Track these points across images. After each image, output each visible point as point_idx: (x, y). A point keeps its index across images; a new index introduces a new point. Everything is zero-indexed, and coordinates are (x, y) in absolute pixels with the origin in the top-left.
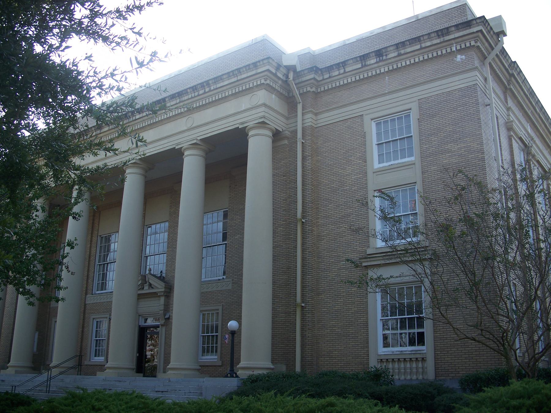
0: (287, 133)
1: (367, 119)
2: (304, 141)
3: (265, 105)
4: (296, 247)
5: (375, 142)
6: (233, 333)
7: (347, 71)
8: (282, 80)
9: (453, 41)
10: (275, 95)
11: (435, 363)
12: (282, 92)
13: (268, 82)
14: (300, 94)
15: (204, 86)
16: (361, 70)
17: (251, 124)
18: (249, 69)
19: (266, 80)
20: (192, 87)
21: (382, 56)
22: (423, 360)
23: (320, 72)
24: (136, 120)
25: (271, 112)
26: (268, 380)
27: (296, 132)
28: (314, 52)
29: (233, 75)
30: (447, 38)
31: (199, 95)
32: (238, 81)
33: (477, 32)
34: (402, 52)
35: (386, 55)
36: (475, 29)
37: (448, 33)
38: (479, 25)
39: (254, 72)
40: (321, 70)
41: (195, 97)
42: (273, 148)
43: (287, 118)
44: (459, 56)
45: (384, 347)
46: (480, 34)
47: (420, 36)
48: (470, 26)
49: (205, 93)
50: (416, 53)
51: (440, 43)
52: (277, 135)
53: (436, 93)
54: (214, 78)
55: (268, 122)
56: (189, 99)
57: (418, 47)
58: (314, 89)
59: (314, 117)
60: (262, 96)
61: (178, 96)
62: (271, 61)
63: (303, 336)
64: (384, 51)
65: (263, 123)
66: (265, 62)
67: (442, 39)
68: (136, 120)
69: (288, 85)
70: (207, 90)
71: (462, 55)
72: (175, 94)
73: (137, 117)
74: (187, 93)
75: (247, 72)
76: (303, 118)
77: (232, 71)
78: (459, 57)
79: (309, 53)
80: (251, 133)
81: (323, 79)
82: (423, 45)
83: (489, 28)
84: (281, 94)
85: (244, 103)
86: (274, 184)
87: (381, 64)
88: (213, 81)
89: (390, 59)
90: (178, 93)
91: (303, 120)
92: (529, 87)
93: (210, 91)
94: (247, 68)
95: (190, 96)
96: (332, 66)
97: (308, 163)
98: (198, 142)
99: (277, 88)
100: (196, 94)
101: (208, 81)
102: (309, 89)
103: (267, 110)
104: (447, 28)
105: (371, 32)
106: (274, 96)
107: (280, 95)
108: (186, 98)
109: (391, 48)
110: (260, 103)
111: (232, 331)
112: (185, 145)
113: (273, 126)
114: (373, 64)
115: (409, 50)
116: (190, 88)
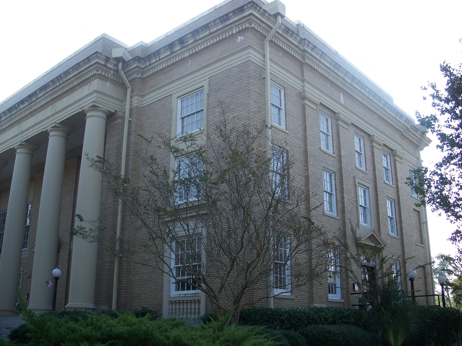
1: (174, 97)
2: (131, 120)
3: (97, 91)
5: (179, 116)
7: (161, 58)
8: (114, 70)
9: (233, 25)
10: (110, 82)
11: (206, 304)
13: (100, 72)
14: (129, 81)
16: (171, 56)
19: (98, 71)
21: (184, 43)
22: (199, 302)
23: (143, 61)
25: (104, 97)
28: (147, 44)
29: (76, 68)
30: (228, 23)
32: (79, 73)
33: (249, 15)
34: (197, 38)
35: (187, 42)
36: (247, 13)
37: (228, 19)
38: (250, 10)
39: (88, 65)
40: (143, 59)
41: (54, 88)
44: (239, 38)
45: (176, 291)
46: (252, 17)
47: (208, 24)
48: (243, 11)
49: (60, 85)
50: (208, 38)
51: (223, 28)
52: (110, 117)
53: (221, 71)
55: (99, 105)
56: (50, 91)
57: (208, 33)
58: (140, 76)
62: (98, 55)
63: (119, 282)
64: (184, 38)
65: (94, 106)
66: (94, 56)
67: (224, 24)
68: (21, 110)
70: (61, 82)
71: (241, 36)
72: (42, 87)
73: (22, 107)
74: (49, 85)
76: (131, 100)
78: (240, 38)
79: (142, 45)
80: (88, 115)
81: (146, 67)
82: (211, 31)
83: (261, 11)
87: (183, 50)
89: (190, 45)
90: (44, 86)
91: (132, 101)
92: (330, 61)
96: (150, 55)
98: (57, 125)
99: (109, 76)
102: (136, 76)
103: (99, 95)
104: (227, 15)
105: (184, 24)
106: (108, 84)
107: (114, 82)
109: (189, 36)
111: (55, 277)
113: (105, 108)
114: (178, 51)
115: (201, 36)
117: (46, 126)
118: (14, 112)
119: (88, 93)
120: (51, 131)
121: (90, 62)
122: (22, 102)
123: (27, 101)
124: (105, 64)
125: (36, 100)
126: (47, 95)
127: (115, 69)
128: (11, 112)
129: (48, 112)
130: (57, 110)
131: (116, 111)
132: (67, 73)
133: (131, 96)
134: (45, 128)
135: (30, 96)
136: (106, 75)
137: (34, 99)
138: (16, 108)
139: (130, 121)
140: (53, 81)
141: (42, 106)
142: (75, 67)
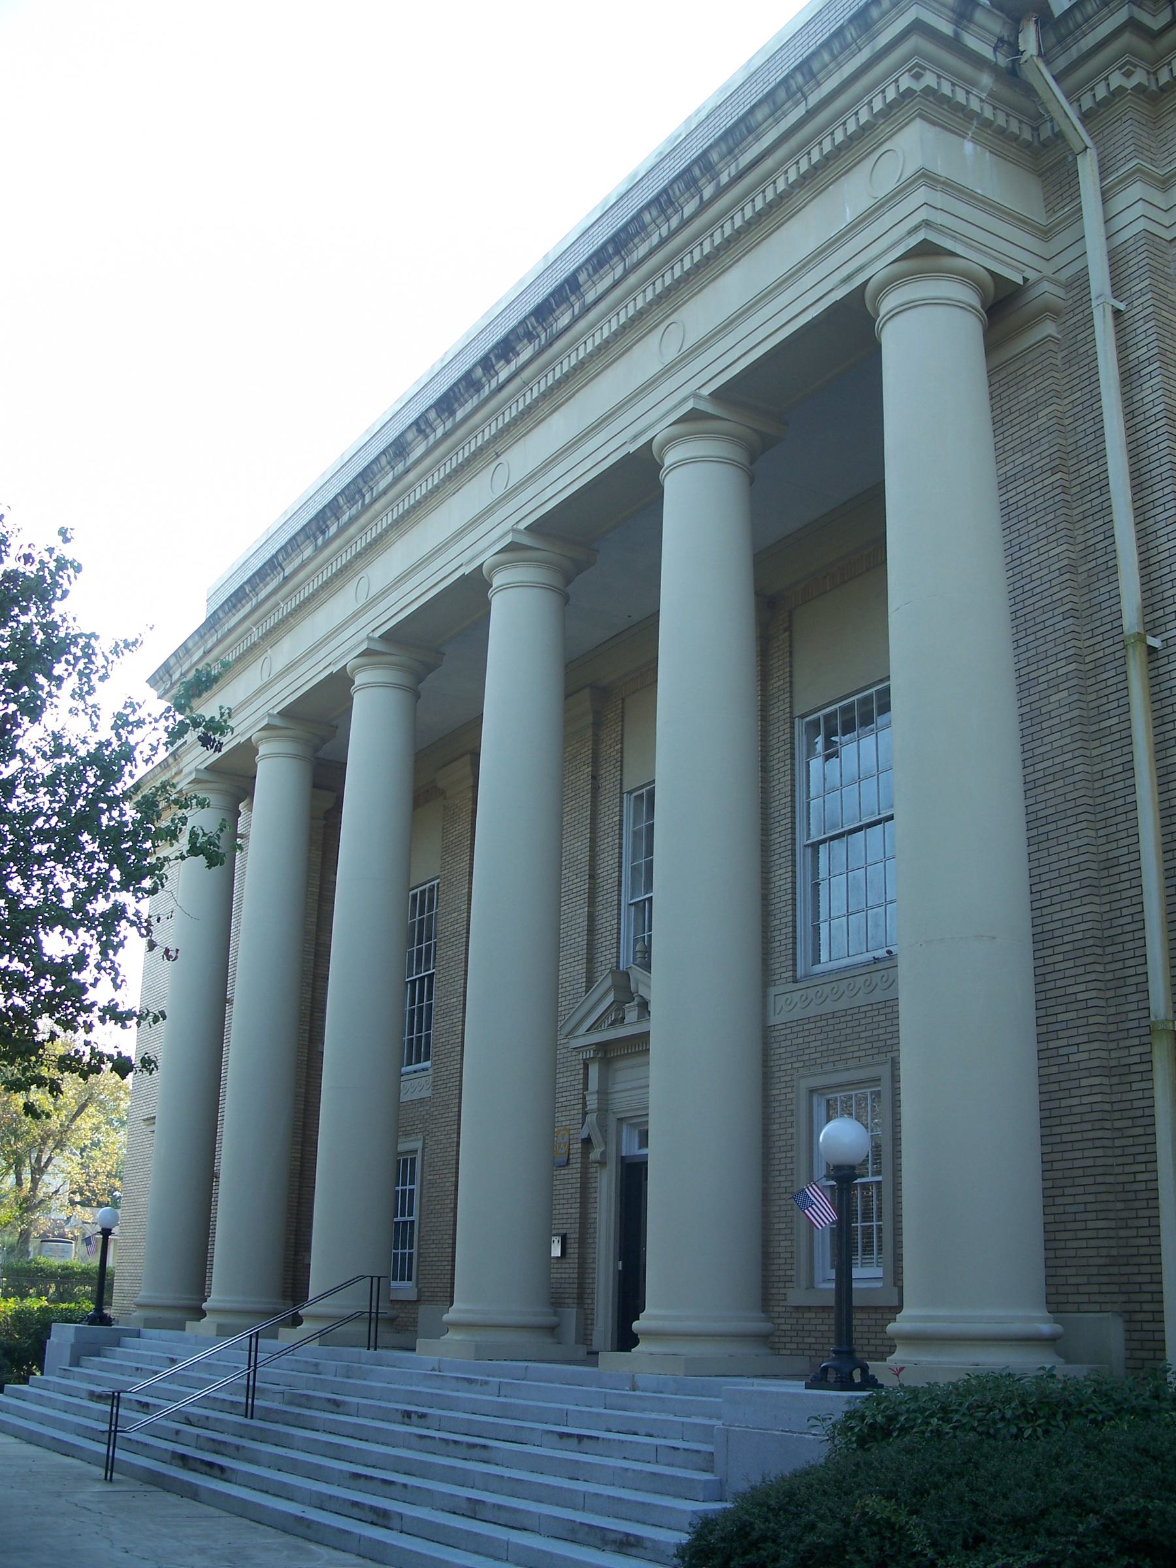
0: (1048, 292)
2: (1122, 306)
4: (1129, 768)
6: (844, 1177)
8: (993, 68)
10: (974, 140)
12: (1001, 120)
13: (929, 80)
14: (1085, 117)
15: (695, 181)
17: (878, 271)
18: (844, 49)
19: (917, 77)
20: (656, 200)
24: (501, 387)
26: (938, 1434)
27: (1081, 281)
29: (790, 96)
31: (684, 223)
32: (811, 114)
41: (673, 234)
42: (991, 373)
43: (1045, 234)
49: (704, 206)
52: (1002, 307)
54: (723, 137)
55: (948, 244)
56: (651, 252)
58: (1139, 77)
59: (1157, 198)
60: (913, 146)
61: (617, 252)
65: (926, 250)
68: (501, 387)
69: (1029, 91)
70: (708, 193)
72: (603, 247)
73: (503, 376)
75: (840, 66)
77: (785, 81)
84: (1002, 132)
85: (852, 194)
86: (1009, 513)
88: (724, 148)
93: (720, 192)
94: (836, 46)
95: (655, 239)
97: (1151, 392)
99: (975, 105)
100: (674, 222)
101: (705, 153)
102: (1116, 80)
103: (939, 198)
106: (968, 147)
107: (999, 140)
108: (643, 250)
110: (909, 172)
111: (837, 1168)
112: (660, 432)
113: (977, 261)
116: (647, 207)
117: (652, 420)
118: (469, 407)
119: (865, 204)
120: (496, 567)
121: (873, 38)
122: (505, 348)
123: (530, 336)
124: (956, 33)
125: (575, 320)
126: (632, 279)
127: (1003, 61)
128: (452, 413)
129: (647, 357)
130: (374, 591)
131: (1025, 280)
132: (739, 132)
133: (1103, 194)
134: (635, 437)
135: (543, 312)
136: (961, 97)
137: (565, 320)
138: (476, 386)
139: (1117, 313)
140: (663, 202)
141: (606, 344)
142: (773, 101)
